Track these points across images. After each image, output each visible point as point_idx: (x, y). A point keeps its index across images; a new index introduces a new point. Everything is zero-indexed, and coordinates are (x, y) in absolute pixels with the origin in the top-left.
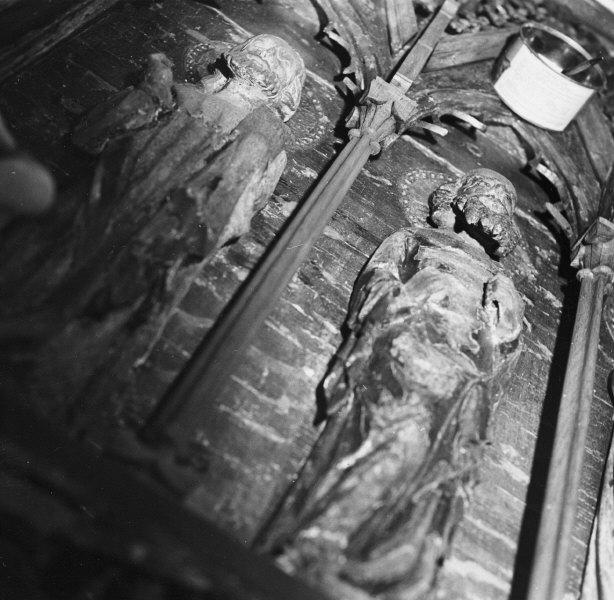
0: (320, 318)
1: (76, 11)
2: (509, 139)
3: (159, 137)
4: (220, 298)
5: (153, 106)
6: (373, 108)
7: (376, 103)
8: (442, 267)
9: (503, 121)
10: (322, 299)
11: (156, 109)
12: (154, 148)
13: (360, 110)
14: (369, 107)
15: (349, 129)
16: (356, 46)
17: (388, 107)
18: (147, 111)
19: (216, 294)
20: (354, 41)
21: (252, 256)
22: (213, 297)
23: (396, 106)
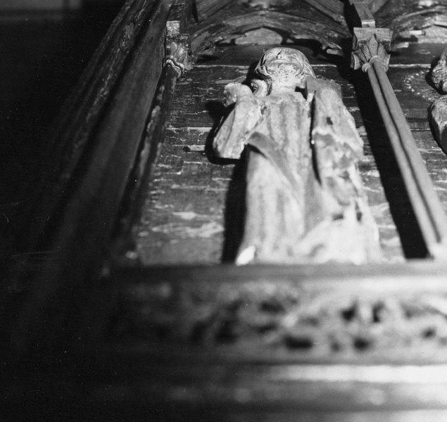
0: (440, 171)
1: (124, 124)
2: (437, 35)
3: (272, 121)
4: (377, 191)
5: (254, 106)
6: (365, 46)
7: (365, 42)
8: (359, 217)
9: (428, 24)
10: (430, 162)
11: (257, 107)
12: (276, 127)
13: (357, 54)
14: (362, 48)
15: (360, 69)
16: (316, 34)
17: (373, 41)
18: (253, 112)
19: (373, 191)
20: (312, 31)
21: (371, 163)
22: (372, 193)
23: (378, 36)
